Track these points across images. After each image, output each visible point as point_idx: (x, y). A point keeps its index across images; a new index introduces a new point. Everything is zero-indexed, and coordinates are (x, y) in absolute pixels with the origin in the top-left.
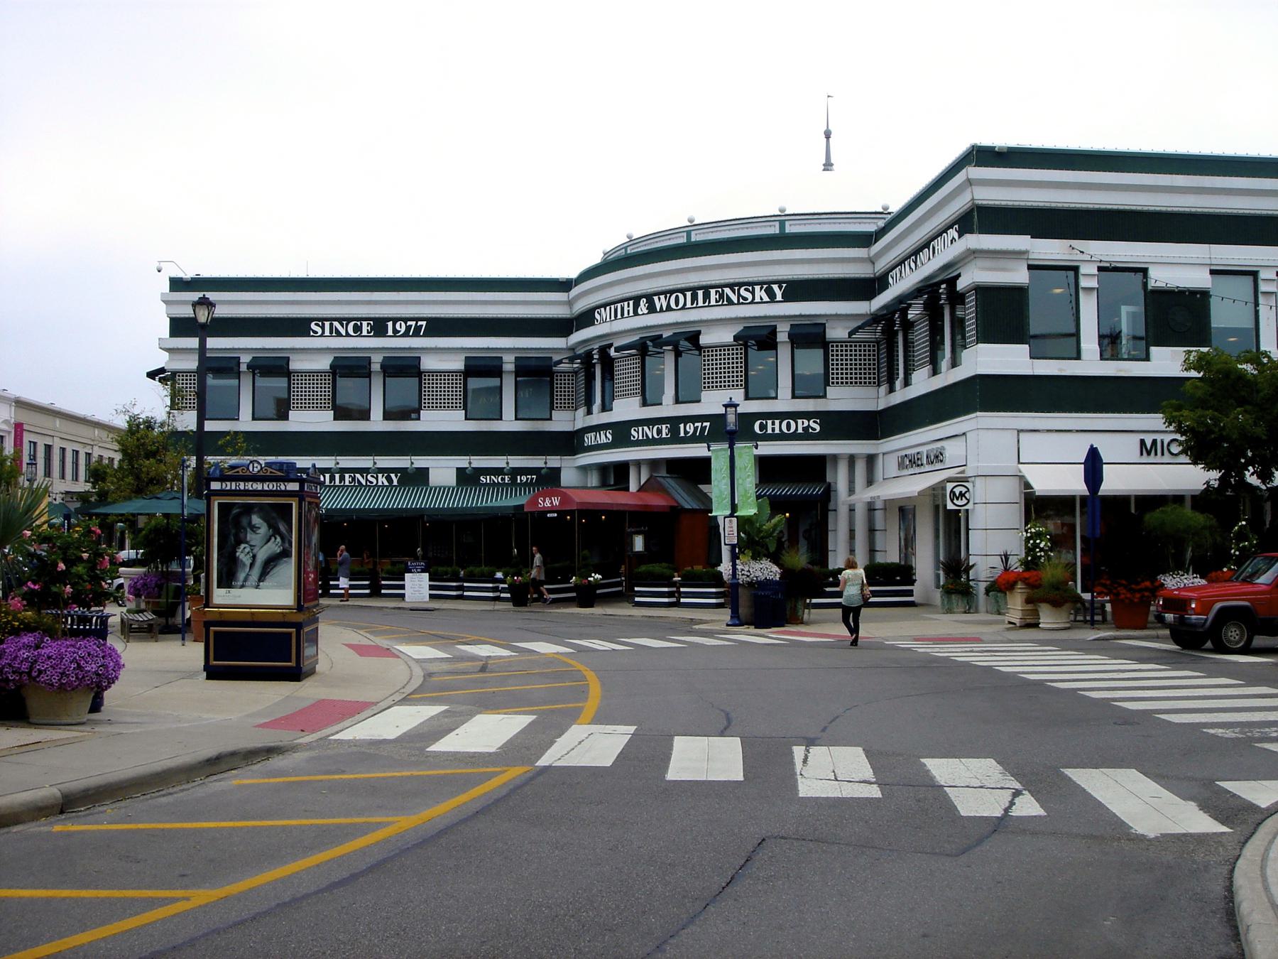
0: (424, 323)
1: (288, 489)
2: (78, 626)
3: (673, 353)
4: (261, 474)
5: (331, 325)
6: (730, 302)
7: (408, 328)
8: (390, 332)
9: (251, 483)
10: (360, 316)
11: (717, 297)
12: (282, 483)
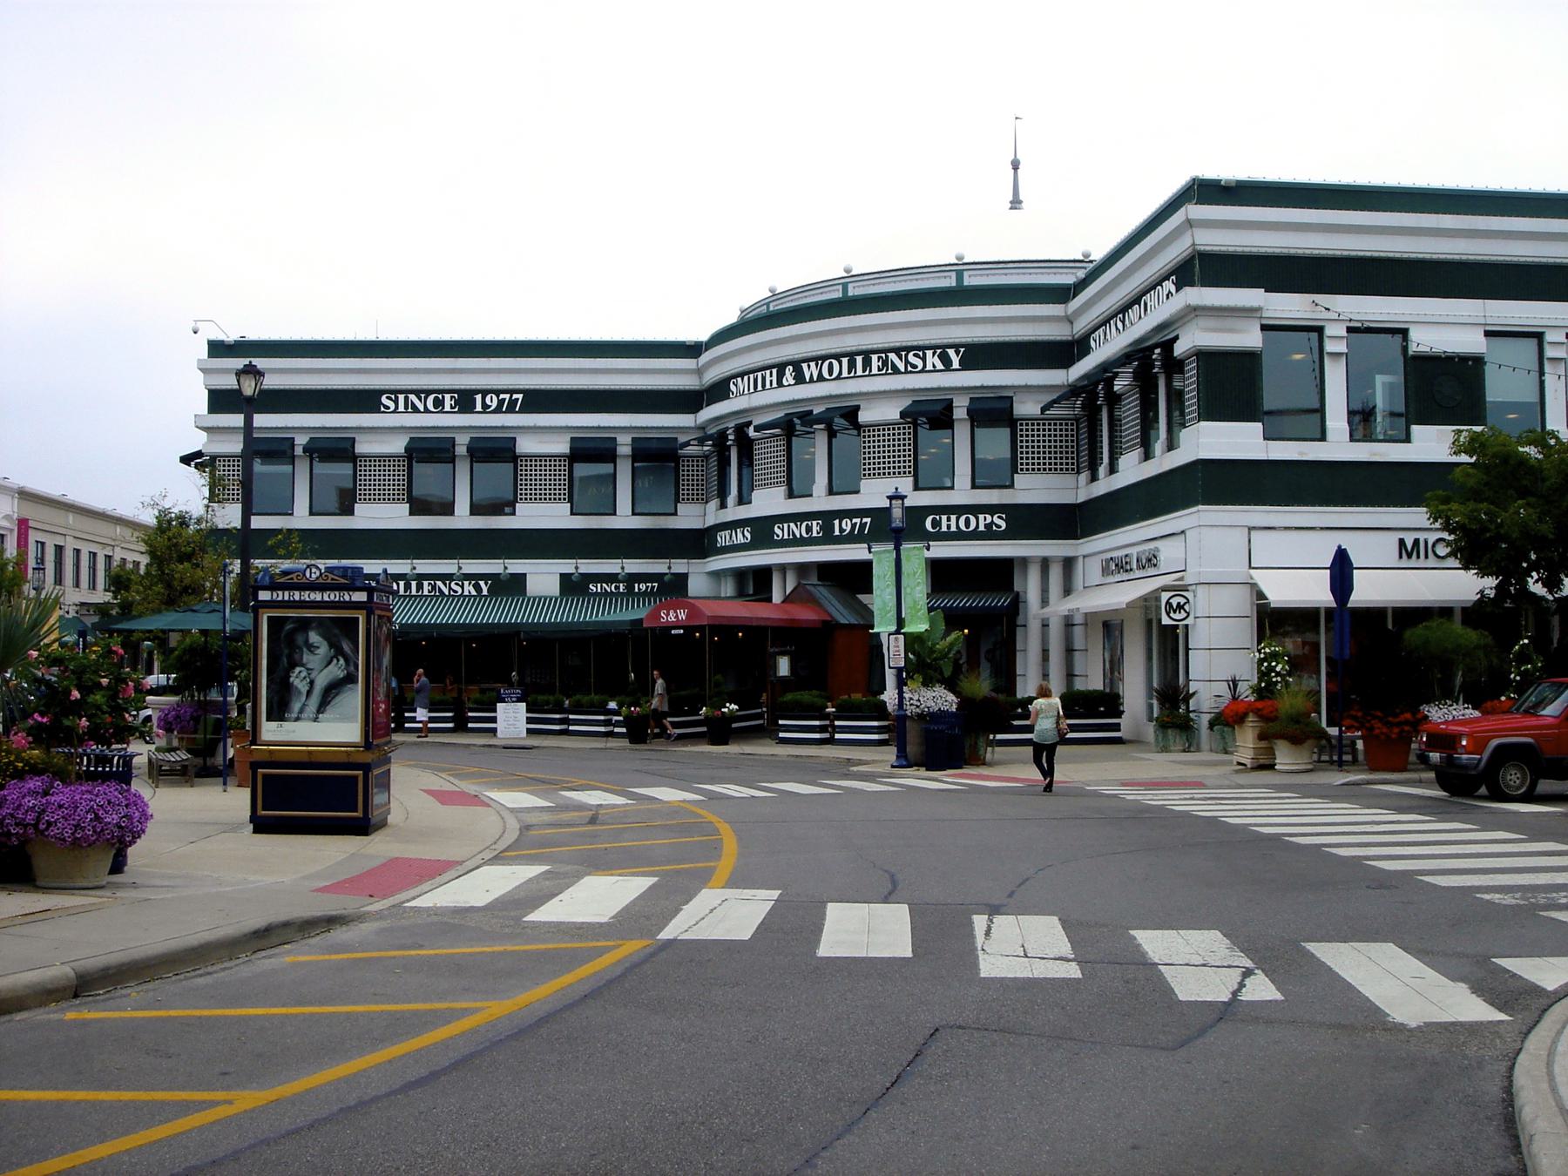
0: (520, 396)
1: (353, 599)
2: (96, 767)
3: (826, 433)
4: (321, 581)
5: (406, 399)
6: (896, 371)
7: (501, 402)
8: (479, 408)
9: (308, 592)
10: (442, 387)
11: (880, 364)
12: (346, 593)
